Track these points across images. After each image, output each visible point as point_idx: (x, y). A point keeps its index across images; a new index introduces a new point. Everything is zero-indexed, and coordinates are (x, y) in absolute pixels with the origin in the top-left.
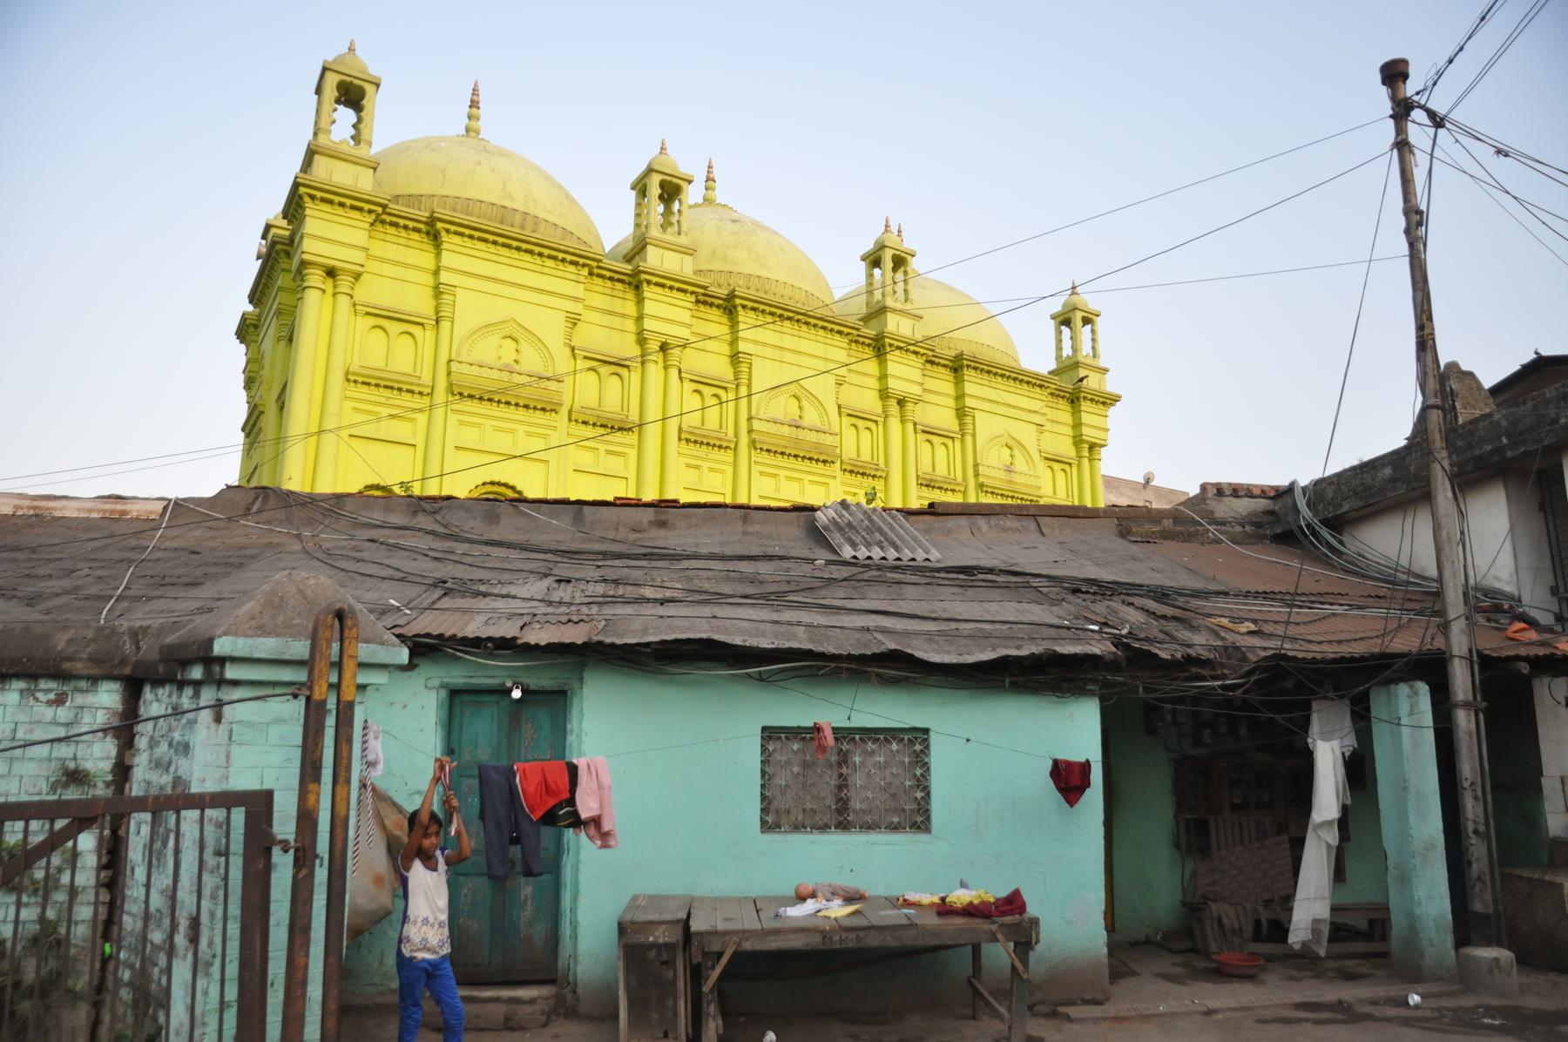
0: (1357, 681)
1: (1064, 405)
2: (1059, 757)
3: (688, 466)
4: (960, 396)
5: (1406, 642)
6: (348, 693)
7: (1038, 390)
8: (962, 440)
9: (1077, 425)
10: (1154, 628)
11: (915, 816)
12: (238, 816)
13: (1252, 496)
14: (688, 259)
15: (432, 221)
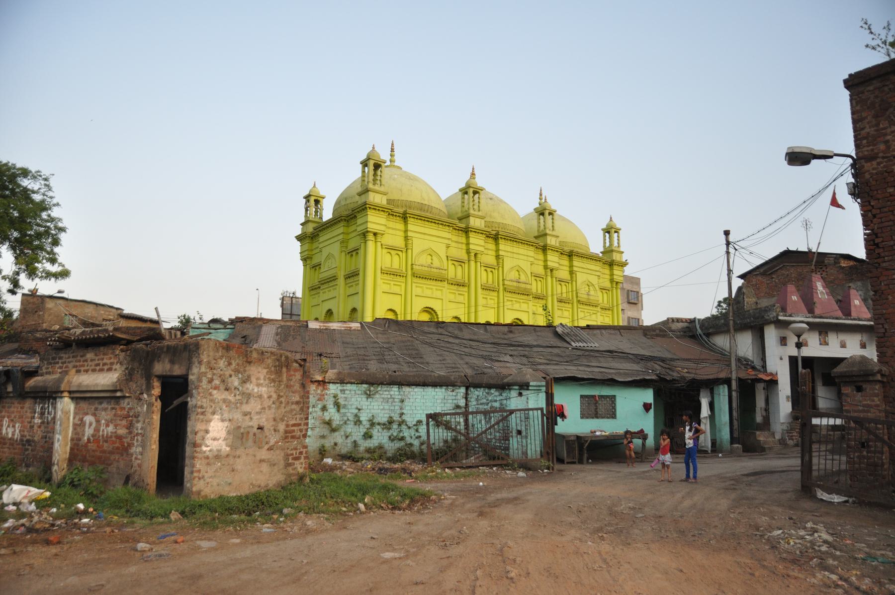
0: (711, 385)
1: (607, 267)
4: (571, 266)
5: (722, 375)
6: (114, 367)
9: (612, 275)
10: (663, 371)
11: (613, 415)
12: (539, 412)
14: (483, 221)
15: (405, 213)
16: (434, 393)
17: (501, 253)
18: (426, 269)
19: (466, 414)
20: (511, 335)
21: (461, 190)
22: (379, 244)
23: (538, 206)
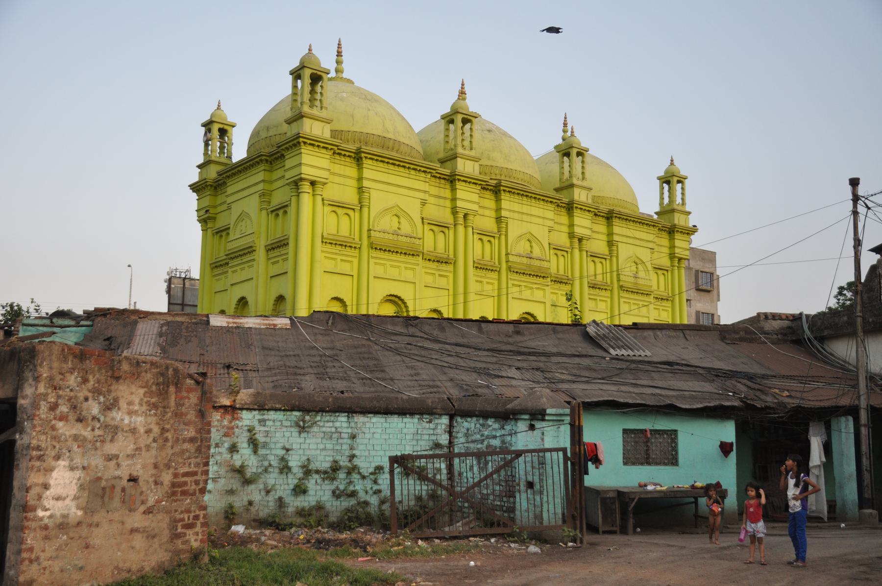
0: (826, 416)
1: (665, 235)
2: (723, 440)
3: (477, 281)
4: (610, 234)
5: (845, 401)
7: (652, 228)
8: (611, 260)
9: (672, 247)
11: (672, 460)
12: (561, 454)
13: (781, 319)
14: (477, 165)
16: (401, 425)
17: (504, 213)
18: (390, 237)
19: (449, 457)
20: (518, 338)
21: (443, 117)
22: (319, 198)
23: (560, 141)
